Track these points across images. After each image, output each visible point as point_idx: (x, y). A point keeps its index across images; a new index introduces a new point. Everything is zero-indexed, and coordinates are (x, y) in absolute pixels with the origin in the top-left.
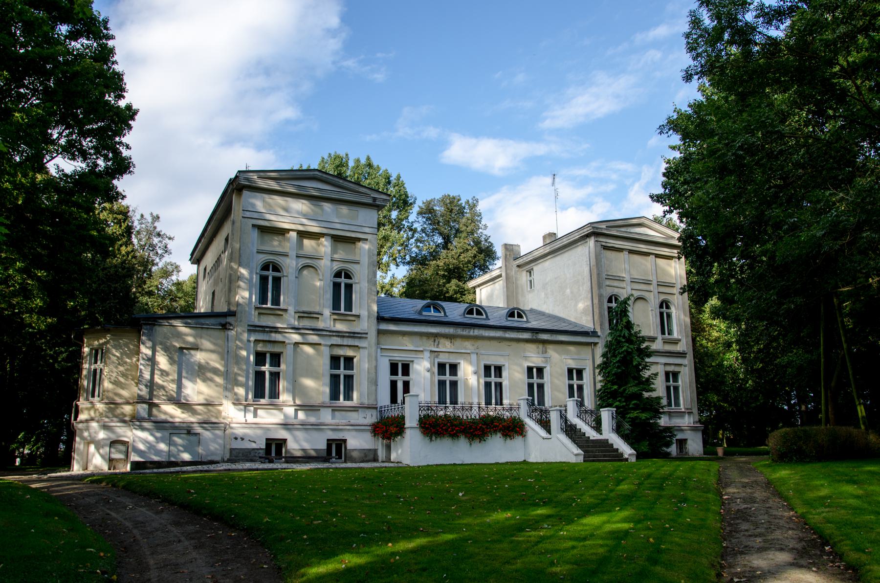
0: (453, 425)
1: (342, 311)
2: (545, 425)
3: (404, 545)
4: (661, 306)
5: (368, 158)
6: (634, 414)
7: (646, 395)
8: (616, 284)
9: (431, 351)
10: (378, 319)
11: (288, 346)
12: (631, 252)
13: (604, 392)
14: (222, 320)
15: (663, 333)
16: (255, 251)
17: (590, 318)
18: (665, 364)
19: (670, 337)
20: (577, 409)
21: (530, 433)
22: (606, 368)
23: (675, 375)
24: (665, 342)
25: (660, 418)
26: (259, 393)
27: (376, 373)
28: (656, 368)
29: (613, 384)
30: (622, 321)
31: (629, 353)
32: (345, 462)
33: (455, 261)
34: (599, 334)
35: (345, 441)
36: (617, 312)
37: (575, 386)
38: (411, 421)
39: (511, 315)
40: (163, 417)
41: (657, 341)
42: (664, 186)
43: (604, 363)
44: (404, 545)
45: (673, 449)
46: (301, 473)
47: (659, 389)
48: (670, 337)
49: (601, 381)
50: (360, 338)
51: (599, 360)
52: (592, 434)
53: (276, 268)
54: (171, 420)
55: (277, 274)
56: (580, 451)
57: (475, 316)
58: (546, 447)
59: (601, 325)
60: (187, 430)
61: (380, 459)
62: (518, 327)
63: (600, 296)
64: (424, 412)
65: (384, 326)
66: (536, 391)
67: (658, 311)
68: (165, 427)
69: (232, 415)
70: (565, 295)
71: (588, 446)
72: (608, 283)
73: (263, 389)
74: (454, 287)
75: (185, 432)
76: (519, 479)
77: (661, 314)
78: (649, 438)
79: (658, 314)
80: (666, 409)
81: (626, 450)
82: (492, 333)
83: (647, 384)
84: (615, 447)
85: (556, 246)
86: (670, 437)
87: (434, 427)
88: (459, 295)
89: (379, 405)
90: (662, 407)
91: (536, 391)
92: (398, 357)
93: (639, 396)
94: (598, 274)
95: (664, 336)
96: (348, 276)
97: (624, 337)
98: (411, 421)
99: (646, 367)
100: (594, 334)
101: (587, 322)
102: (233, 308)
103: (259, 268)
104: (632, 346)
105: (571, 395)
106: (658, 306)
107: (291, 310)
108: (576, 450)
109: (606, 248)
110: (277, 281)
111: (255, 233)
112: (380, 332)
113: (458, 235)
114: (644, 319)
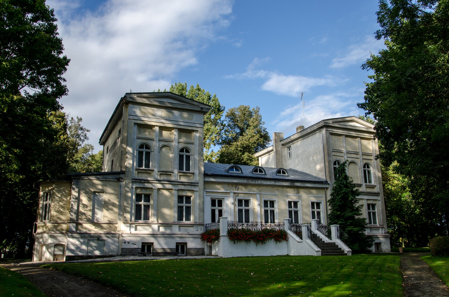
0: (246, 234)
1: (184, 171)
2: (299, 234)
4: (364, 167)
6: (350, 228)
7: (357, 217)
8: (338, 154)
12: (347, 136)
15: (366, 182)
16: (136, 137)
17: (323, 174)
18: (367, 200)
19: (370, 184)
20: (317, 225)
21: (290, 239)
22: (333, 202)
23: (373, 206)
24: (367, 187)
25: (365, 231)
26: (138, 217)
27: (203, 205)
28: (362, 202)
29: (338, 211)
30: (342, 175)
32: (186, 255)
34: (329, 182)
38: (223, 232)
39: (279, 172)
41: (362, 186)
43: (332, 199)
45: (373, 249)
46: (162, 262)
47: (364, 214)
48: (370, 184)
51: (329, 198)
52: (326, 239)
53: (148, 147)
54: (89, 232)
55: (148, 150)
56: (319, 249)
57: (258, 173)
58: (300, 247)
59: (330, 178)
60: (98, 238)
61: (206, 254)
62: (281, 179)
63: (329, 162)
65: (207, 179)
66: (293, 215)
67: (363, 169)
68: (86, 237)
70: (308, 160)
71: (324, 247)
72: (334, 154)
73: (140, 215)
75: (97, 239)
77: (365, 171)
78: (359, 242)
79: (363, 171)
80: (368, 226)
81: (346, 249)
82: (268, 183)
85: (305, 133)
87: (236, 236)
88: (249, 162)
90: (366, 224)
91: (293, 215)
92: (217, 196)
93: (352, 218)
95: (366, 184)
96: (187, 151)
97: (343, 184)
98: (223, 232)
99: (356, 201)
100: (326, 182)
101: (322, 176)
102: (124, 170)
103: (138, 147)
104: (348, 190)
105: (313, 217)
106: (363, 167)
108: (317, 249)
111: (136, 128)
112: (205, 182)
113: (248, 128)
114: (355, 174)
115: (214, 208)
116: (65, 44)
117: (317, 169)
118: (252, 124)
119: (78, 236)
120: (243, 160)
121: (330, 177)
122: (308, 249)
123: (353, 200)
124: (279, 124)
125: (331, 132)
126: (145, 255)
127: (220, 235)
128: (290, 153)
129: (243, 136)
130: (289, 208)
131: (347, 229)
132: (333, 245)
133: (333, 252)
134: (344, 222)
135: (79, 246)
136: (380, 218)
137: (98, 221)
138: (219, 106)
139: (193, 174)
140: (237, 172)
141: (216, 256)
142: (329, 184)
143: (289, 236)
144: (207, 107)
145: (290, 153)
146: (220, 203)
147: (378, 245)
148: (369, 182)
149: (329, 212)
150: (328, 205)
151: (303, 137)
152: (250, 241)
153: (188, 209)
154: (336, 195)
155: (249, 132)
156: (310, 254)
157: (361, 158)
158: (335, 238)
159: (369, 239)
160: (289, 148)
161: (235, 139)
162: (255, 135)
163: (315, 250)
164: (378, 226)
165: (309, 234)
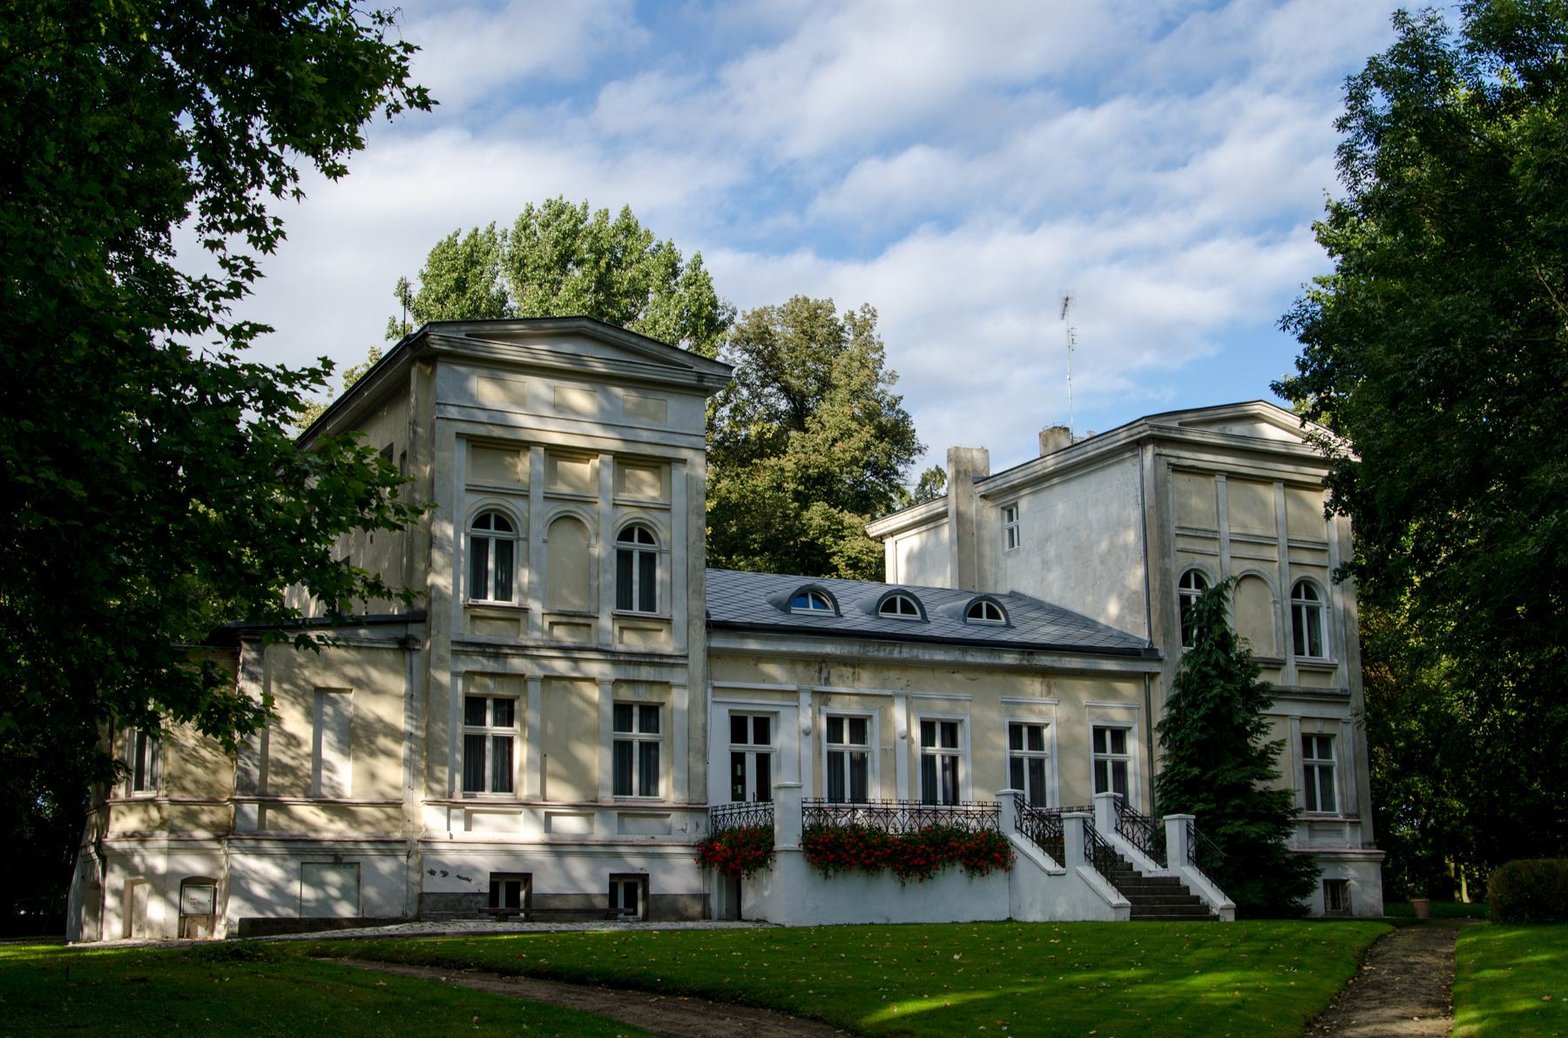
0: (868, 847)
1: (636, 611)
2: (1053, 846)
3: (912, 1007)
4: (1296, 593)
5: (626, 213)
6: (1236, 826)
7: (1259, 786)
8: (1198, 545)
9: (814, 693)
11: (531, 685)
12: (1232, 476)
13: (1171, 782)
14: (399, 632)
15: (1299, 650)
16: (463, 487)
17: (1141, 619)
18: (1303, 719)
19: (1315, 660)
20: (1114, 815)
21: (1021, 864)
22: (1176, 730)
23: (1325, 742)
24: (1304, 670)
25: (1288, 835)
26: (474, 783)
27: (705, 737)
28: (1282, 729)
29: (1192, 764)
30: (1210, 631)
31: (1225, 700)
32: (646, 918)
33: (822, 459)
34: (1161, 654)
36: (1200, 613)
37: (1109, 765)
38: (787, 836)
39: (974, 611)
40: (297, 829)
41: (1284, 669)
42: (1302, 366)
43: (1172, 719)
44: (912, 1007)
45: (1317, 901)
46: (599, 939)
47: (1288, 773)
48: (1315, 660)
49: (1164, 758)
50: (673, 665)
51: (1160, 714)
52: (1145, 866)
53: (503, 523)
54: (313, 835)
55: (647, 547)
56: (1123, 900)
57: (899, 614)
58: (1058, 892)
59: (1165, 635)
60: (339, 856)
61: (715, 913)
62: (990, 639)
63: (1165, 574)
64: (812, 820)
65: (719, 642)
66: (1027, 774)
67: (1288, 603)
68: (306, 852)
69: (430, 819)
70: (1089, 565)
71: (1140, 892)
72: (1181, 543)
73: (481, 773)
74: (817, 521)
75: (331, 860)
76: (1034, 939)
77: (1296, 610)
78: (1265, 876)
79: (1289, 611)
80: (1301, 817)
81: (1217, 899)
82: (939, 655)
83: (1262, 762)
84: (1192, 893)
85: (1075, 461)
86: (1308, 874)
87: (833, 851)
88: (829, 539)
89: (711, 804)
90: (1294, 813)
91: (1027, 774)
92: (754, 705)
93: (1244, 789)
94: (1162, 526)
95: (1300, 658)
96: (646, 537)
97: (1216, 665)
98: (787, 836)
99: (1259, 728)
100: (1150, 654)
101: (1139, 630)
102: (420, 604)
103: (470, 522)
104: (1230, 687)
105: (1101, 786)
106: (1288, 593)
108: (1117, 899)
109: (1178, 469)
112: (712, 655)
113: (827, 395)
114: (1256, 624)
115: (739, 747)
117: (1117, 605)
118: (844, 380)
119: (276, 851)
120: (805, 533)
121: (1166, 635)
122: (1083, 896)
123: (1248, 722)
124: (970, 413)
125: (1173, 460)
126: (503, 917)
127: (776, 848)
128: (1011, 531)
129: (806, 431)
130: (1012, 747)
131: (1222, 830)
133: (1172, 911)
134: (1213, 806)
135: (282, 883)
136: (1347, 788)
137: (339, 796)
138: (714, 305)
139: (668, 621)
140: (821, 612)
141: (758, 921)
142: (1160, 660)
143: (1017, 854)
144: (721, 372)
145: (1011, 531)
146: (763, 730)
147: (1336, 889)
148: (1312, 654)
149: (1159, 770)
150: (1156, 742)
151: (1064, 473)
152: (878, 869)
153: (650, 750)
154: (1188, 706)
155: (832, 413)
156: (1090, 917)
157: (1285, 561)
158: (1177, 864)
159: (1300, 865)
160: (1010, 512)
161: (776, 446)
162: (854, 426)
163: (1109, 903)
164: (1341, 818)
165: (1090, 846)
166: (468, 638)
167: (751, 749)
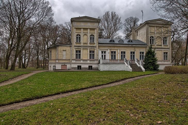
10: (99, 43)
14: (70, 45)
18: (164, 51)
35: (92, 66)
39: (129, 41)
55: (80, 36)
65: (100, 45)
81: (143, 69)
103: (76, 35)
107: (82, 43)
110: (80, 38)
111: (75, 29)
116: (107, 10)
130: (140, 54)
132: (140, 68)
146: (105, 52)
166: (76, 45)
167: (104, 54)
